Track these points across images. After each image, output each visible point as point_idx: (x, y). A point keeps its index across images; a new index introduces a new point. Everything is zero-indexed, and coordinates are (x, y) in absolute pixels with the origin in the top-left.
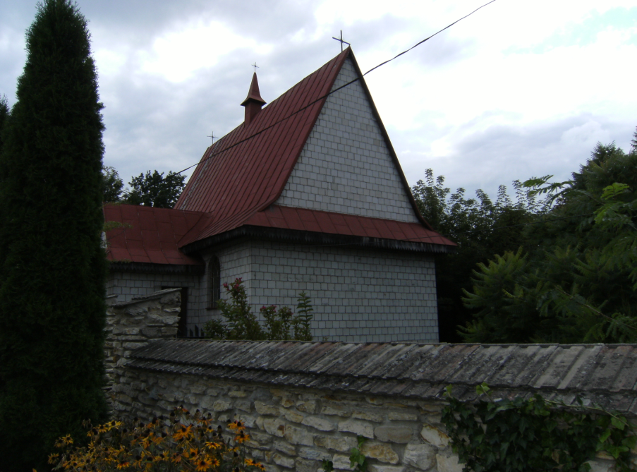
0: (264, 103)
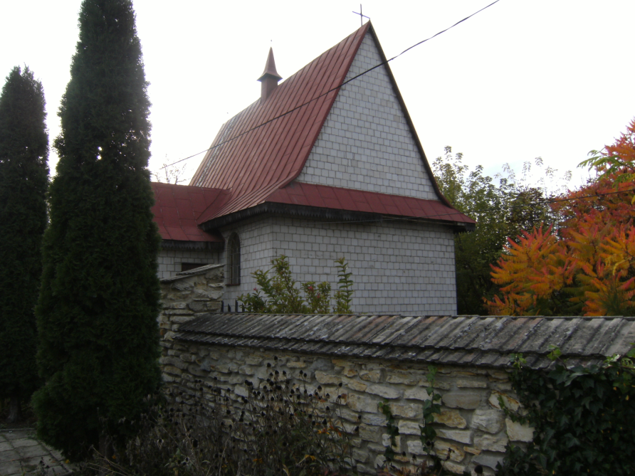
0: (280, 78)
